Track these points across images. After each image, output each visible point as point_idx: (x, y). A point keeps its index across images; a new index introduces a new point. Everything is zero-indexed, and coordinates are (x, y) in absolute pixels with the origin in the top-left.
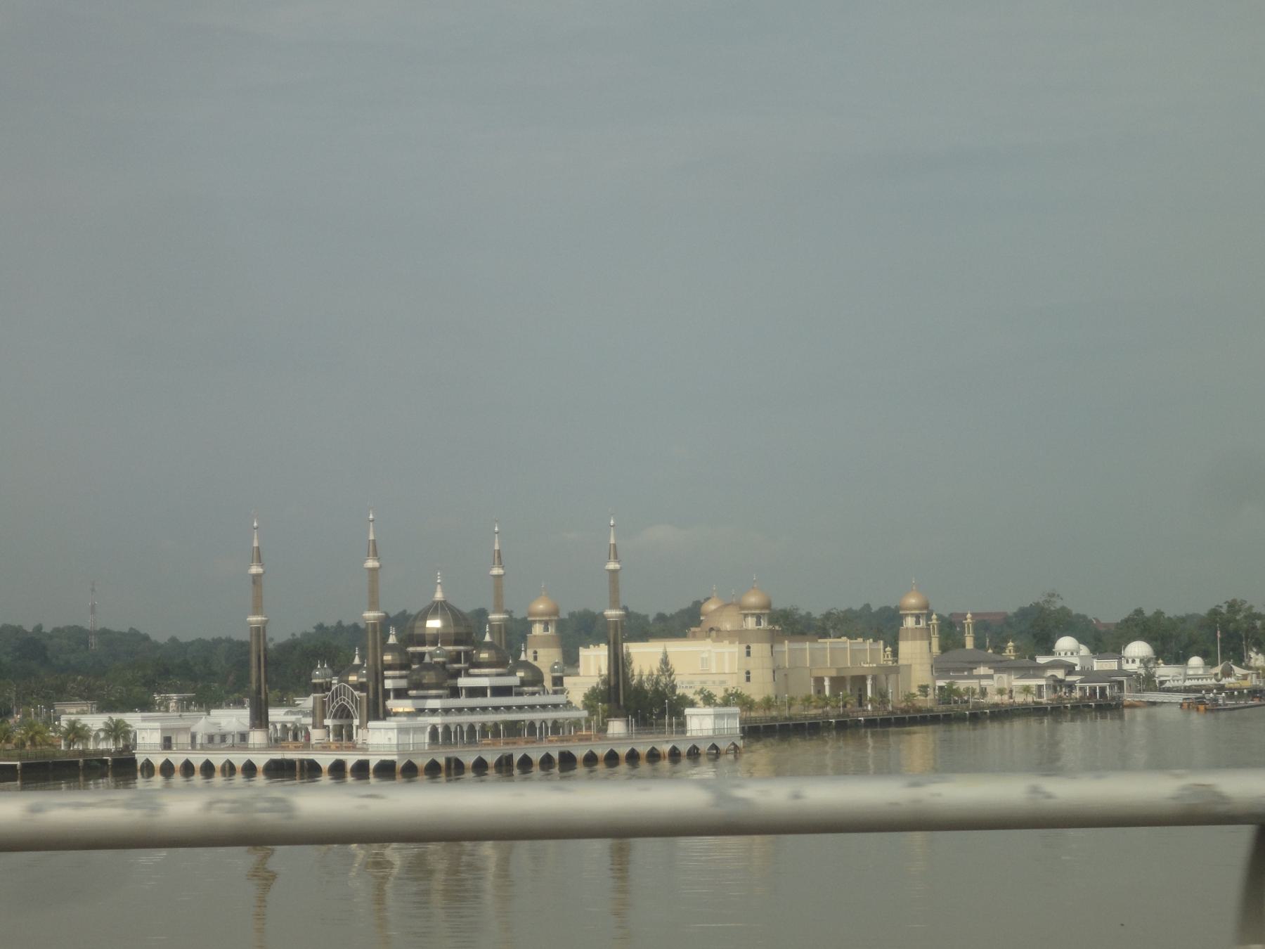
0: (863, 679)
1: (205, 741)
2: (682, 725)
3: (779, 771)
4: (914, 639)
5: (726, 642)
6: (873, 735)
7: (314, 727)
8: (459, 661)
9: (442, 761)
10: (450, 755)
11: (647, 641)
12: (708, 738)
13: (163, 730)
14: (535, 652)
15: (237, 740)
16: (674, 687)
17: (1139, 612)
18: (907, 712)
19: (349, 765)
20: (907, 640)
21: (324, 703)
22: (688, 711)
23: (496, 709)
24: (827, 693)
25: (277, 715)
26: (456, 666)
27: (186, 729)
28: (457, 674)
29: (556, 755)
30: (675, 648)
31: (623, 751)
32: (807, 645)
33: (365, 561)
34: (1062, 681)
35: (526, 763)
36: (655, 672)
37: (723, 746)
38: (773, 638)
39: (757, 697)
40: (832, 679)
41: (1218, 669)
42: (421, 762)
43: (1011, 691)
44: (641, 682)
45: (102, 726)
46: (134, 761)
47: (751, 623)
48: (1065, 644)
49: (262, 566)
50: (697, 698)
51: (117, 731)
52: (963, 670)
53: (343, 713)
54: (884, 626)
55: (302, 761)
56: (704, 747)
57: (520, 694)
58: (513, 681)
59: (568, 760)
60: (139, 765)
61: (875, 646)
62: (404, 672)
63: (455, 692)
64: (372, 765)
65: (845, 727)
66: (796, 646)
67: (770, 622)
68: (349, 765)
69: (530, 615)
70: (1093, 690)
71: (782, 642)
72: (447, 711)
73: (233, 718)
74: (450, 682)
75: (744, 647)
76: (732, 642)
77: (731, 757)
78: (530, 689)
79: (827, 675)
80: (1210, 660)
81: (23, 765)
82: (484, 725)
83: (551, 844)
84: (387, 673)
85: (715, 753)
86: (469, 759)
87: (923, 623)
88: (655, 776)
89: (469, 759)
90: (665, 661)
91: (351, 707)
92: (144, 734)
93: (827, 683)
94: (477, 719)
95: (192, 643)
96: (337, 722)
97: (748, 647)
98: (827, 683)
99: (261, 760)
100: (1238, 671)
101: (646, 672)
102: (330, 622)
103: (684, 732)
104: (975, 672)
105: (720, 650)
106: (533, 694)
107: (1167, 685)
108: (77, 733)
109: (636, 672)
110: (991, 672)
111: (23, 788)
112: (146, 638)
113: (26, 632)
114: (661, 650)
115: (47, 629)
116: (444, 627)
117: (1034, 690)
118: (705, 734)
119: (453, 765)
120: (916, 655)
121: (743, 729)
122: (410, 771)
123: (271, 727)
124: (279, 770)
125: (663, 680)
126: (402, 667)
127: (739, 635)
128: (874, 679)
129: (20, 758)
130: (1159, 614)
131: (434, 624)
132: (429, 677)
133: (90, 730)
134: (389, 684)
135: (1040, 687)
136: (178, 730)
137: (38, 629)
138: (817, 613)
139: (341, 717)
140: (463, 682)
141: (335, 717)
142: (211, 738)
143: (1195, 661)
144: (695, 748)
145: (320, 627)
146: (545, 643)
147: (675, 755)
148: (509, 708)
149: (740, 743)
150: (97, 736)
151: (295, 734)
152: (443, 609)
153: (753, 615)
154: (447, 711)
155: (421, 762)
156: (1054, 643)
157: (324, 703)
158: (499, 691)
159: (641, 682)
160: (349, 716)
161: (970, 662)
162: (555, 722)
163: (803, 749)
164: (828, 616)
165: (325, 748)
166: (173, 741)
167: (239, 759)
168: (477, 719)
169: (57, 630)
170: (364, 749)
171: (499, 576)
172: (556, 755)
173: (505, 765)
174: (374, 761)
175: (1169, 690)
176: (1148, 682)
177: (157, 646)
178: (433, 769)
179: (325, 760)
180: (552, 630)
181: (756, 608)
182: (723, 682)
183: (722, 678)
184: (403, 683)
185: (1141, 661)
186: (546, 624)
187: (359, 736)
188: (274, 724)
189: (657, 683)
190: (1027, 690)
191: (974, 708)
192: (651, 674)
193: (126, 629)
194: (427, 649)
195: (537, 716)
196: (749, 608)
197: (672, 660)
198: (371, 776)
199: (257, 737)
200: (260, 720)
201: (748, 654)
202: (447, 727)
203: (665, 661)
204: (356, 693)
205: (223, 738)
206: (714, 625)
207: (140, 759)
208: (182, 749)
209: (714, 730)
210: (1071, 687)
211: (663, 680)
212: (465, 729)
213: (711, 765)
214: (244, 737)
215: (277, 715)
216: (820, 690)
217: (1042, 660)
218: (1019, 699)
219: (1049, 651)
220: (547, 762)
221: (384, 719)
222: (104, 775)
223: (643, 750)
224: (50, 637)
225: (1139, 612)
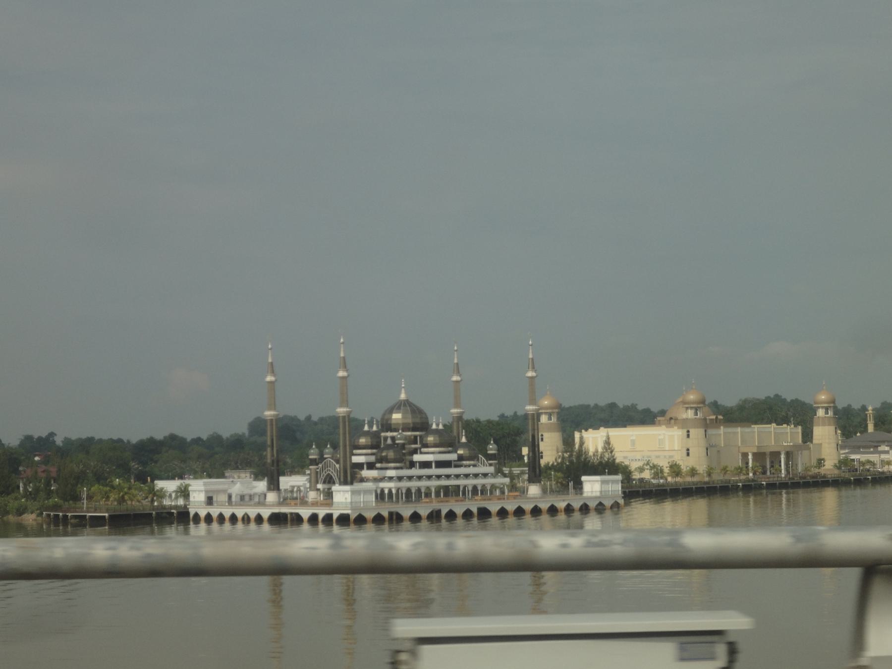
0: (775, 455)
1: (239, 499)
3: (713, 523)
4: (824, 425)
6: (787, 493)
9: (385, 514)
10: (392, 510)
11: (625, 426)
12: (596, 498)
13: (206, 492)
17: (850, 406)
18: (804, 478)
19: (321, 517)
20: (819, 425)
21: (317, 473)
23: (439, 477)
26: (413, 446)
27: (224, 491)
28: (415, 451)
29: (475, 510)
31: (544, 506)
32: (739, 429)
33: (337, 372)
35: (451, 516)
36: (600, 450)
37: (608, 503)
38: (706, 425)
40: (754, 454)
42: (370, 515)
46: (188, 513)
47: (690, 414)
49: (535, 371)
52: (869, 447)
54: (800, 414)
55: (291, 514)
56: (592, 505)
57: (456, 466)
58: (453, 457)
59: (484, 514)
61: (795, 430)
62: (374, 451)
63: (412, 465)
64: (335, 517)
65: (749, 488)
66: (730, 430)
68: (321, 517)
69: (815, 403)
71: (719, 427)
72: (400, 479)
74: (408, 458)
75: (685, 431)
78: (468, 462)
79: (751, 451)
81: (110, 516)
83: (466, 576)
85: (600, 508)
86: (406, 512)
87: (700, 415)
88: (452, 530)
89: (406, 512)
90: (607, 442)
91: (335, 476)
93: (750, 457)
96: (326, 486)
97: (688, 431)
98: (750, 457)
99: (266, 513)
102: (509, 413)
103: (582, 494)
104: (880, 449)
105: (670, 433)
111: (110, 534)
113: (299, 420)
114: (605, 434)
115: (315, 418)
116: (403, 417)
118: (594, 494)
119: (394, 517)
120: (825, 435)
121: (624, 493)
122: (361, 520)
124: (277, 520)
126: (372, 447)
127: (684, 424)
128: (788, 455)
129: (107, 511)
131: (397, 416)
132: (391, 454)
134: (356, 459)
136: (218, 492)
137: (309, 418)
140: (417, 458)
141: (324, 482)
142: (242, 498)
144: (600, 504)
145: (502, 416)
146: (550, 429)
147: (519, 512)
148: (448, 477)
149: (621, 502)
150: (170, 496)
152: (405, 405)
153: (691, 408)
154: (400, 479)
155: (370, 515)
157: (317, 473)
158: (440, 464)
163: (734, 505)
164: (627, 409)
166: (215, 499)
167: (253, 512)
169: (322, 419)
171: (457, 382)
172: (475, 510)
173: (434, 517)
174: (336, 514)
178: (378, 519)
180: (831, 413)
181: (825, 403)
183: (671, 453)
184: (372, 459)
186: (827, 409)
193: (495, 418)
195: (461, 482)
196: (821, 403)
197: (612, 441)
198: (334, 524)
199: (271, 497)
200: (274, 485)
201: (688, 436)
203: (607, 442)
205: (251, 497)
206: (673, 415)
207: (192, 512)
208: (221, 505)
209: (601, 492)
211: (607, 455)
212: (404, 491)
213: (598, 516)
215: (286, 482)
220: (468, 515)
222: (171, 523)
224: (316, 423)
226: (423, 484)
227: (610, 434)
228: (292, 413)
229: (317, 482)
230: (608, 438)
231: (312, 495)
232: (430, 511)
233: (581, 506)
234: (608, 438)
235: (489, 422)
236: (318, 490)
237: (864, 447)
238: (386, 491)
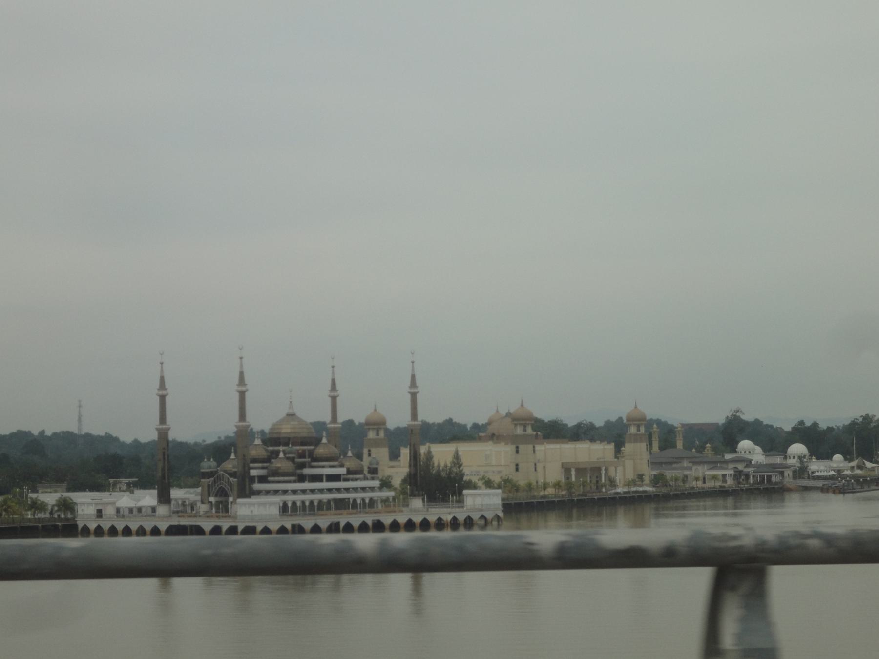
2: (461, 502)
5: (503, 444)
7: (203, 502)
8: (304, 457)
10: (295, 523)
14: (369, 451)
15: (150, 510)
16: (462, 475)
17: (802, 423)
20: (630, 442)
21: (209, 486)
22: (465, 492)
23: (330, 490)
24: (573, 479)
25: (177, 494)
27: (114, 503)
28: (302, 466)
30: (466, 449)
34: (741, 471)
36: (449, 465)
39: (522, 483)
41: (854, 464)
42: (274, 526)
43: (704, 479)
44: (439, 472)
45: (54, 502)
46: (76, 526)
48: (745, 444)
50: (480, 483)
51: (67, 506)
53: (223, 493)
55: (191, 526)
57: (269, 482)
60: (80, 529)
63: (302, 479)
67: (534, 430)
70: (763, 478)
73: (148, 498)
74: (299, 471)
75: (513, 447)
76: (506, 444)
77: (495, 523)
80: (848, 456)
82: (320, 502)
84: (252, 465)
90: (457, 457)
91: (227, 488)
92: (83, 507)
93: (573, 472)
94: (316, 497)
95: (148, 443)
96: (218, 499)
97: (517, 447)
98: (573, 472)
99: (163, 526)
100: (869, 465)
101: (442, 465)
106: (356, 480)
107: (816, 474)
108: (37, 506)
109: (436, 464)
110: (690, 465)
112: (116, 439)
115: (49, 433)
117: (721, 478)
119: (297, 529)
123: (173, 502)
124: (174, 531)
125: (455, 470)
130: (815, 425)
133: (47, 505)
134: (254, 473)
135: (724, 476)
137: (42, 433)
138: (571, 423)
139: (221, 496)
140: (307, 471)
141: (216, 496)
143: (838, 457)
148: (338, 490)
149: (501, 515)
151: (186, 508)
156: (737, 443)
159: (439, 472)
160: (226, 495)
161: (677, 458)
162: (371, 500)
164: (579, 426)
165: (207, 516)
168: (316, 497)
169: (55, 434)
170: (235, 517)
175: (814, 478)
176: (801, 472)
177: (123, 445)
179: (207, 526)
182: (499, 472)
185: (800, 458)
187: (232, 509)
188: (176, 500)
189: (450, 472)
190: (714, 478)
191: (676, 490)
192: (446, 466)
193: (102, 434)
194: (281, 448)
195: (351, 496)
199: (162, 510)
200: (164, 498)
201: (517, 452)
202: (312, 502)
203: (457, 457)
204: (231, 479)
205: (140, 510)
210: (747, 476)
214: (154, 509)
215: (177, 494)
216: (568, 478)
217: (728, 457)
218: (710, 484)
219: (734, 450)
221: (249, 496)
223: (432, 519)
224: (50, 438)
225: (802, 423)
226: (298, 498)
227: (432, 449)
228: (25, 429)
229: (209, 496)
230: (457, 452)
231: (203, 508)
232: (328, 524)
233: (465, 520)
234: (457, 452)
235: (99, 436)
236: (211, 502)
237: (666, 463)
238: (307, 504)
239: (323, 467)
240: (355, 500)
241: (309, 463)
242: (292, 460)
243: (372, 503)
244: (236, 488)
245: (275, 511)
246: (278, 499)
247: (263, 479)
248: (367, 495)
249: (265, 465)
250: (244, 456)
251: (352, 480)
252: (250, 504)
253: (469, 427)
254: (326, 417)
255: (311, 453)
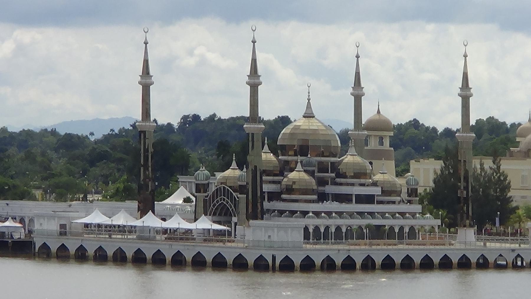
21: (205, 201)
23: (361, 214)
28: (322, 182)
63: (323, 197)
73: (275, 238)
74: (321, 188)
92: (42, 221)
139: (220, 215)
140: (330, 189)
148: (372, 214)
162: (412, 228)
195: (387, 223)
239: (353, 185)
240: (392, 228)
241: (333, 179)
242: (311, 173)
243: (413, 233)
244: (242, 206)
245: (299, 236)
246: (303, 222)
247: (274, 196)
248: (407, 223)
249: (276, 178)
250: (256, 167)
251: (389, 202)
252: (267, 228)
253: (485, 120)
254: (512, 187)
255: (334, 167)
